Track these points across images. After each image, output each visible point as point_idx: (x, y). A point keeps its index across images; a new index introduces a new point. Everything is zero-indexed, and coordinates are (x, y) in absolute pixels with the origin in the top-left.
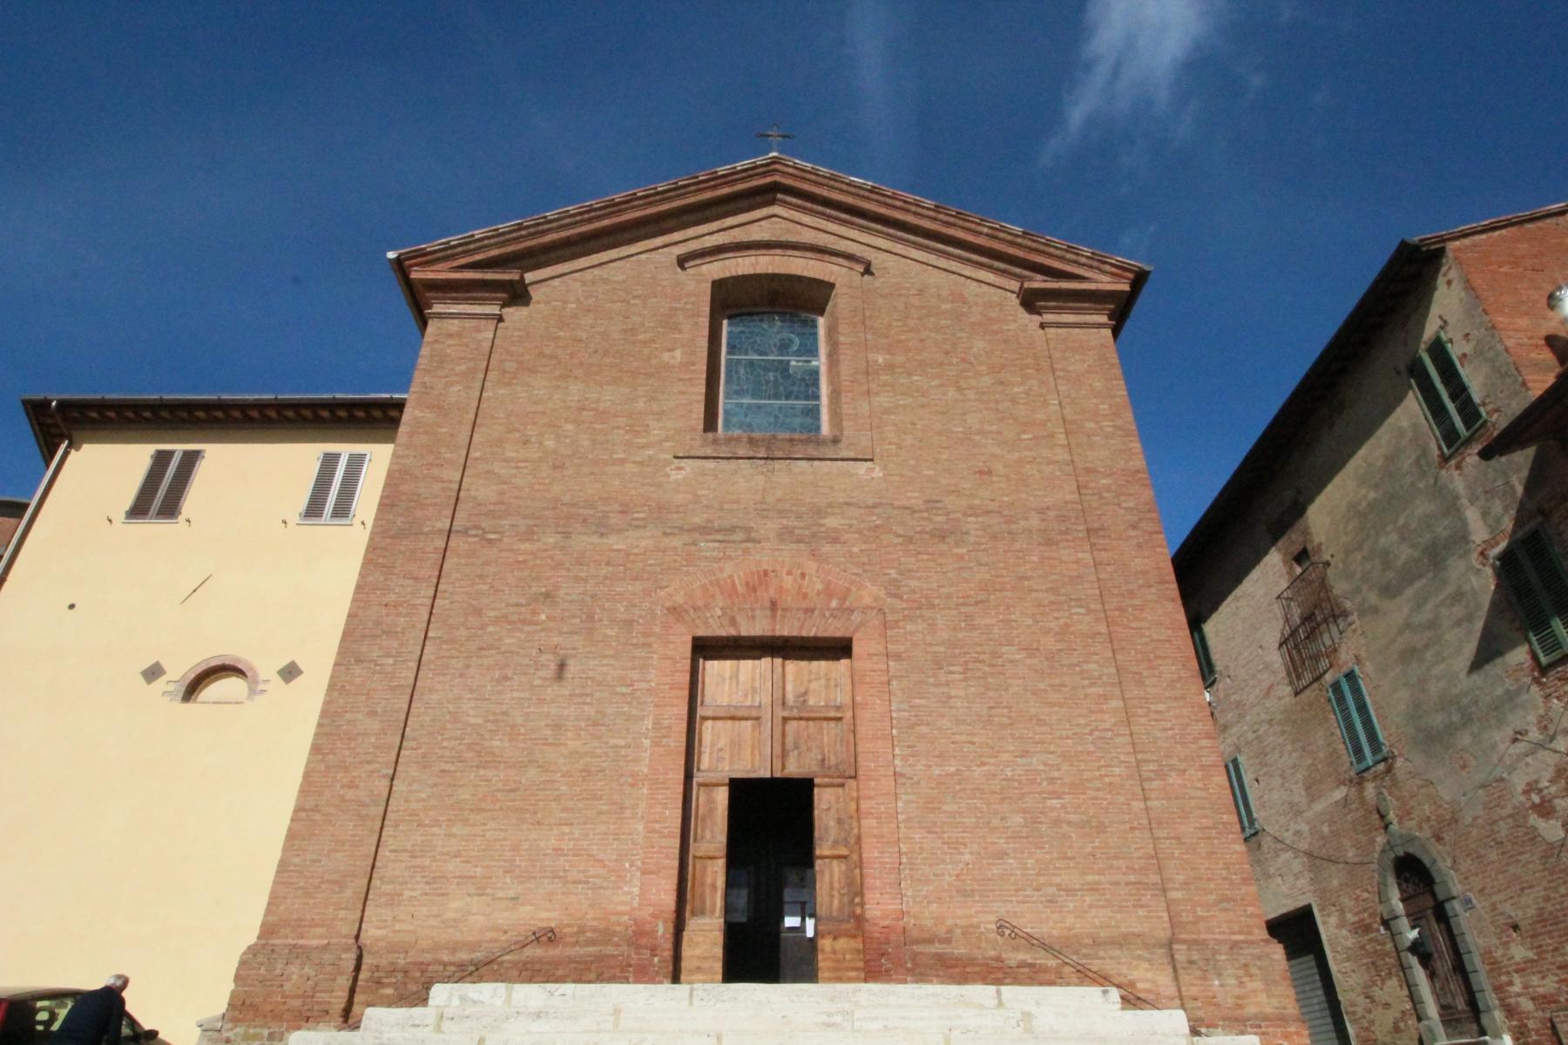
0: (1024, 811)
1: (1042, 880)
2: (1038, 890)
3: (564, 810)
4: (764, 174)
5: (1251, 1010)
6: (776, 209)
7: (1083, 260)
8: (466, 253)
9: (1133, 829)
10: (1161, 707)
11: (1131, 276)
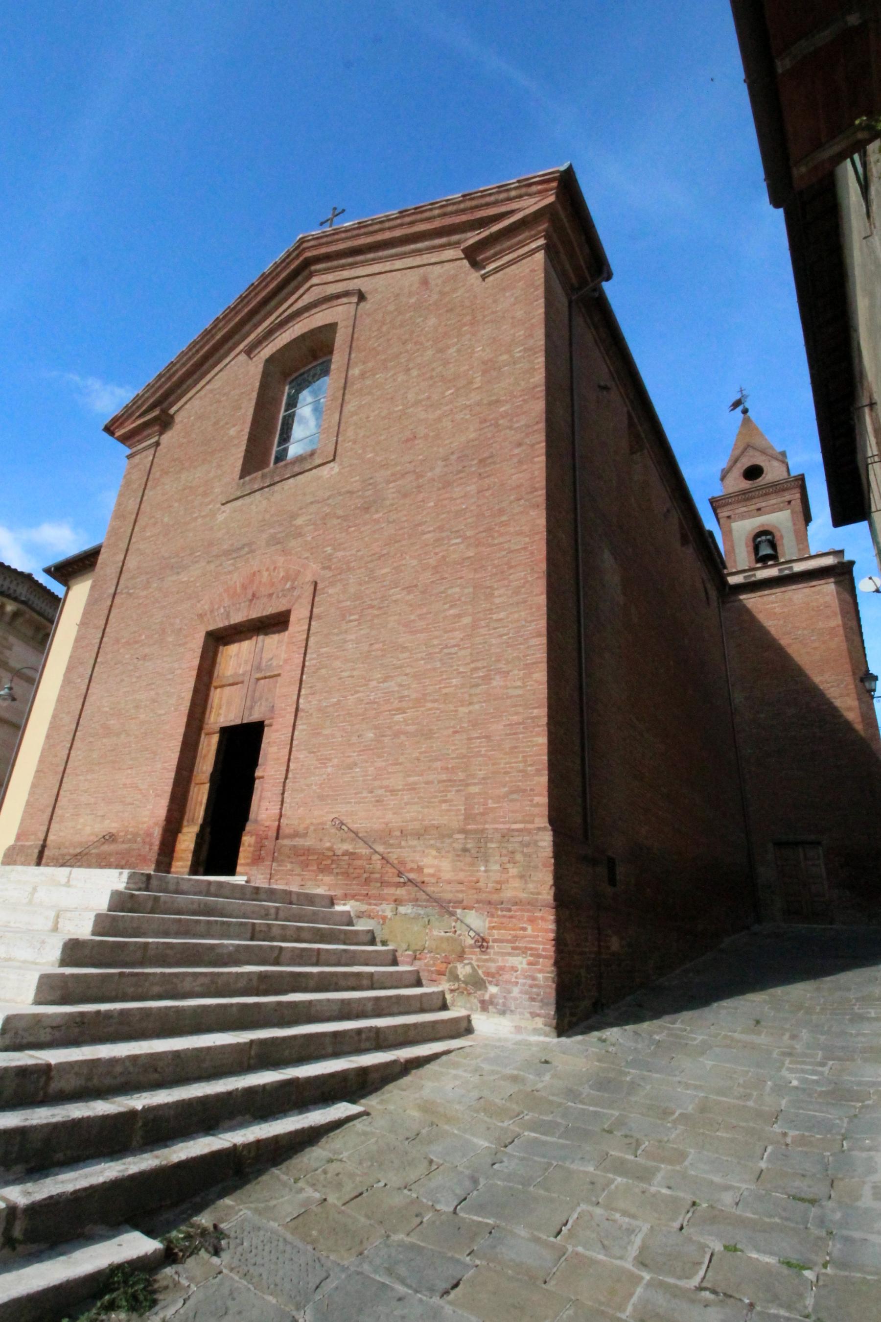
0: (376, 727)
1: (377, 783)
2: (372, 792)
3: (132, 759)
4: (298, 256)
5: (508, 893)
6: (315, 280)
7: (513, 193)
8: (139, 407)
9: (455, 732)
10: (502, 615)
11: (554, 184)
